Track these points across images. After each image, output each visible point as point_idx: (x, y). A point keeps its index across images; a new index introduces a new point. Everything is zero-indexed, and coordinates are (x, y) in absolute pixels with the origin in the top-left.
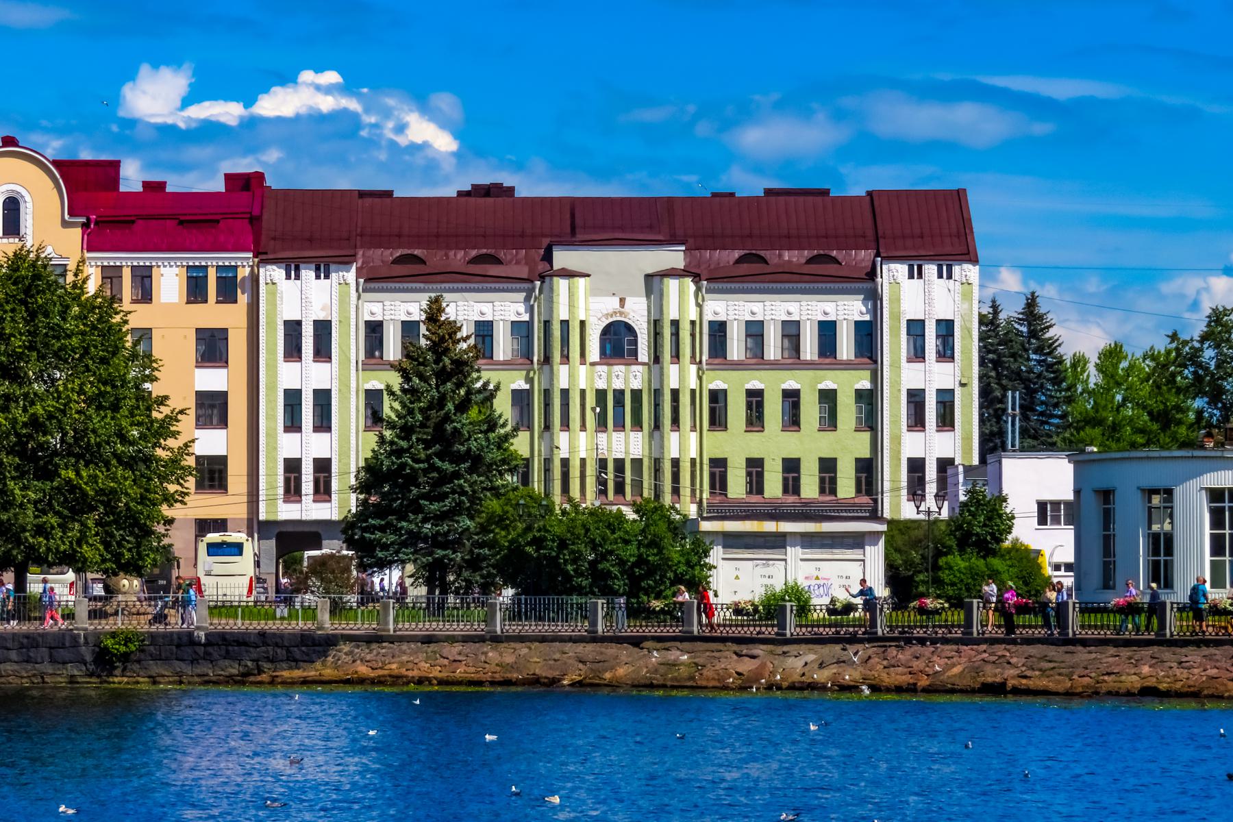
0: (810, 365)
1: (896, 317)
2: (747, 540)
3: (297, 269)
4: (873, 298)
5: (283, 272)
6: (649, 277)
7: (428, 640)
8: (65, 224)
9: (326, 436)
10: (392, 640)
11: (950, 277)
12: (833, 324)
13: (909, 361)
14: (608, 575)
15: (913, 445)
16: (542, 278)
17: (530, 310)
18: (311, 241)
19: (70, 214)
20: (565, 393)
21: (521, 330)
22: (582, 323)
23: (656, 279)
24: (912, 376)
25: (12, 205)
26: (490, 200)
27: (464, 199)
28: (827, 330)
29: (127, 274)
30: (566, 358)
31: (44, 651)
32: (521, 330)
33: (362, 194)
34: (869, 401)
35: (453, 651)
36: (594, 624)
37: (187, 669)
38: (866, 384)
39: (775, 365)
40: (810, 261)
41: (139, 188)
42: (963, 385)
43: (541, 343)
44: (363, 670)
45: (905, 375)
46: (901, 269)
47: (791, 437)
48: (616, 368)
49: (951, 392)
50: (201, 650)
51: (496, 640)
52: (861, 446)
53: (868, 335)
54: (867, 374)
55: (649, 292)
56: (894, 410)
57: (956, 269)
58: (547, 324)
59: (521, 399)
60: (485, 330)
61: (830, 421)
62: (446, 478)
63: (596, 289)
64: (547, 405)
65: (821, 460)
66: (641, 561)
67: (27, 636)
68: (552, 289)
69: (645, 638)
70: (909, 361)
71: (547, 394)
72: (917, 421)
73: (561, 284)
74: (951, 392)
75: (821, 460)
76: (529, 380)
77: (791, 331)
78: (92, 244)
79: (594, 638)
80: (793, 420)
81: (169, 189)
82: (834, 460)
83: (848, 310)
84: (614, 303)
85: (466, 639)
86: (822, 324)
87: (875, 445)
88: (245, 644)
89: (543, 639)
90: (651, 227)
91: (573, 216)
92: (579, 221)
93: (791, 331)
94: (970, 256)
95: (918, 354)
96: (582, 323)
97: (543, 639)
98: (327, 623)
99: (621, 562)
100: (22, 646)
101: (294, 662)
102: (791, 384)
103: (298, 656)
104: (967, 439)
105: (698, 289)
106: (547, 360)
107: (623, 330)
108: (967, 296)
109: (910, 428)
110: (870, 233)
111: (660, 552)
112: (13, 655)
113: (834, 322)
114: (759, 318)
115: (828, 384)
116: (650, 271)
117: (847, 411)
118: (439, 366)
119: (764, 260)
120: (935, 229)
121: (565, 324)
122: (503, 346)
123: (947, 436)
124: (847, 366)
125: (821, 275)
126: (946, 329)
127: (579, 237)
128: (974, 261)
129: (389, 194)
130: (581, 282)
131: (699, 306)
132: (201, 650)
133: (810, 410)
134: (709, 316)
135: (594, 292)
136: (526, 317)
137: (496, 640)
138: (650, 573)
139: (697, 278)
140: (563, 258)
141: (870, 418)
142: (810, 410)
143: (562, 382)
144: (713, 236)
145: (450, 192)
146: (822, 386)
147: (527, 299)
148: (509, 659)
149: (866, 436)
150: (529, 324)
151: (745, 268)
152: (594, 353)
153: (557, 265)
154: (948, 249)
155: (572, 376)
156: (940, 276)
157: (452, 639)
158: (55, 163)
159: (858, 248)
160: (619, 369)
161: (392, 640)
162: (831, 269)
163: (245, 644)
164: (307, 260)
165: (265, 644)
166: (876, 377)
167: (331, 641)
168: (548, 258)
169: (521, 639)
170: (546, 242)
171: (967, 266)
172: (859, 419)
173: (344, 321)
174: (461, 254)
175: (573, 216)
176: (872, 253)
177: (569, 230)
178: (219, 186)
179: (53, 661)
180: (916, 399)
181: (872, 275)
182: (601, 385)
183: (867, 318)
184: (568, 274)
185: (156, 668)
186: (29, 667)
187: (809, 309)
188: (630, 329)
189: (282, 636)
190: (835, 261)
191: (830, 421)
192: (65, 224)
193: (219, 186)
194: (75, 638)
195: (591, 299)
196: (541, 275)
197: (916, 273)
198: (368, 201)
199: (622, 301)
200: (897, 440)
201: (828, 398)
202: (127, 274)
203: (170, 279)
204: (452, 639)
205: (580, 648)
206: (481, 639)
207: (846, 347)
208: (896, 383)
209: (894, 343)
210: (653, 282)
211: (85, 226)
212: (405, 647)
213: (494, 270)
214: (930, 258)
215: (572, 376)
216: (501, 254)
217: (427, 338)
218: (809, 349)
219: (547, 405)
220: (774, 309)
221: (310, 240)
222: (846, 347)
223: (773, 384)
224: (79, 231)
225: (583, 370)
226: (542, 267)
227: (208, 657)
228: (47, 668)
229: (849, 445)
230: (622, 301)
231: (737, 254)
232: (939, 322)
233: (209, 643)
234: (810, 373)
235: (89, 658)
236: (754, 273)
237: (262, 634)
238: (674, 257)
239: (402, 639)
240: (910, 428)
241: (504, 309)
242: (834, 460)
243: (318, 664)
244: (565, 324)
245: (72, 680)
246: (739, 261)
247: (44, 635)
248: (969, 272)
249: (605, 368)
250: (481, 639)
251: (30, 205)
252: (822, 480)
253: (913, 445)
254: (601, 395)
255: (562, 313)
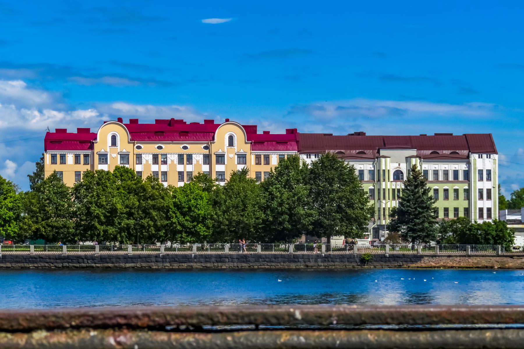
0: (451, 182)
1: (475, 169)
2: (520, 230)
3: (310, 155)
4: (469, 164)
5: (306, 156)
6: (407, 158)
7: (449, 256)
8: (246, 143)
9: (490, 201)
10: (439, 256)
11: (490, 158)
12: (457, 171)
13: (479, 181)
14: (489, 239)
15: (480, 204)
16: (377, 158)
17: (374, 167)
18: (313, 148)
19: (248, 140)
20: (384, 190)
21: (372, 172)
22: (389, 170)
23: (409, 158)
24: (480, 185)
25: (114, 138)
26: (360, 136)
27: (350, 136)
28: (456, 173)
29: (58, 156)
30: (384, 180)
31: (346, 259)
32: (372, 172)
33: (325, 135)
34: (467, 192)
35: (458, 259)
36: (498, 252)
37: (383, 263)
38: (467, 187)
39: (442, 182)
40: (451, 153)
41: (75, 132)
42: (494, 187)
43: (377, 176)
44: (433, 264)
45: (478, 185)
46: (476, 156)
47: (446, 202)
48: (398, 183)
49: (490, 190)
50: (387, 259)
51: (469, 256)
52: (465, 204)
53: (467, 174)
54: (467, 184)
55: (407, 162)
56: (475, 195)
57: (492, 156)
58: (379, 171)
59: (372, 191)
60: (361, 172)
61: (457, 197)
62: (420, 213)
63: (393, 162)
64: (379, 193)
65: (444, 208)
66: (497, 235)
67: (341, 255)
68: (380, 161)
69: (514, 256)
70: (479, 181)
71: (379, 190)
72: (481, 197)
73: (383, 160)
74: (490, 190)
75: (444, 208)
76: (374, 186)
77: (446, 173)
78: (253, 149)
79: (498, 256)
80: (446, 197)
81: (68, 132)
82: (458, 208)
83: (462, 167)
84: (397, 165)
85: (460, 256)
86: (454, 171)
87: (469, 204)
88: (399, 257)
89: (483, 256)
90: (406, 144)
91: (384, 141)
92: (386, 142)
93: (446, 173)
94: (495, 152)
95: (481, 179)
96: (389, 170)
97: (483, 256)
98: (421, 252)
99: (493, 236)
100: (340, 258)
101: (412, 262)
102: (446, 187)
103: (413, 260)
104: (495, 203)
105: (420, 161)
106: (379, 180)
107: (399, 172)
108: (495, 163)
109: (479, 199)
110: (467, 146)
111: (503, 233)
112: (338, 260)
113: (363, 170)
114: (362, 169)
115: (456, 187)
116: (407, 156)
117: (462, 195)
118: (416, 182)
119: (438, 153)
120: (484, 145)
121: (384, 171)
122: (367, 177)
123: (489, 201)
124: (461, 182)
125: (454, 158)
126: (489, 172)
127: (387, 147)
128: (497, 153)
129: (331, 135)
130: (388, 159)
131: (421, 166)
132: (387, 259)
133: (451, 194)
134: (423, 169)
135: (392, 162)
136: (373, 169)
137: (469, 256)
138: (500, 239)
139: (420, 158)
140: (383, 152)
141: (468, 197)
142: (451, 194)
143: (383, 187)
144: (347, 146)
145: (345, 134)
146: (454, 188)
147: (373, 164)
148: (476, 261)
149: (467, 201)
150: (374, 171)
151: (433, 155)
152: (392, 179)
153: (381, 155)
154: (489, 150)
155: (386, 185)
156: (487, 158)
157: (456, 256)
158: (243, 126)
159: (464, 150)
160: (399, 183)
161: (439, 256)
162: (457, 156)
163: (399, 257)
164: (312, 153)
165: (404, 257)
166: (469, 185)
167: (422, 257)
168: (379, 152)
169: (477, 256)
170: (377, 148)
171: (495, 155)
172: (465, 197)
173: (495, 170)
174: (354, 151)
175: (384, 141)
176: (468, 151)
177: (383, 145)
178: (284, 133)
179: (348, 262)
180: (481, 192)
181: (468, 157)
182: (394, 187)
183: (467, 169)
184: (385, 157)
185: (376, 264)
186: (342, 263)
187: (451, 167)
188: (402, 173)
189: (409, 255)
190: (458, 153)
191: (457, 197)
192: (246, 143)
193: (284, 133)
194: (354, 256)
195: (391, 164)
196: (376, 158)
197: (480, 157)
198: (327, 137)
199: (399, 165)
200: (475, 203)
201: (456, 191)
202: (58, 156)
203: (70, 158)
204: (456, 256)
205: (495, 258)
206: (465, 256)
207: (461, 177)
208: (475, 187)
209: (474, 176)
210: (408, 159)
211: (251, 143)
212: (443, 258)
213: (364, 156)
214: (484, 153)
215: (386, 185)
216: (365, 151)
217: (412, 176)
218: (441, 178)
219: (379, 193)
220: (441, 167)
221: (313, 147)
222: (461, 177)
223: (441, 187)
224: (250, 145)
225: (389, 183)
226: (377, 155)
227: (389, 261)
228: (347, 263)
229: (462, 204)
230: (399, 165)
231: (430, 151)
232: (487, 170)
233: (389, 257)
234: (451, 184)
235: (358, 261)
236: (435, 157)
237: (403, 255)
238: (414, 152)
239: (441, 256)
240: (479, 199)
241: (366, 166)
242: (458, 208)
243: (419, 263)
244: (384, 171)
245: (353, 267)
246: (431, 153)
247: (346, 255)
248: (496, 156)
249: (395, 183)
250: (465, 256)
251: (119, 139)
252: (455, 214)
253: (480, 204)
254: (394, 190)
255: (383, 167)
